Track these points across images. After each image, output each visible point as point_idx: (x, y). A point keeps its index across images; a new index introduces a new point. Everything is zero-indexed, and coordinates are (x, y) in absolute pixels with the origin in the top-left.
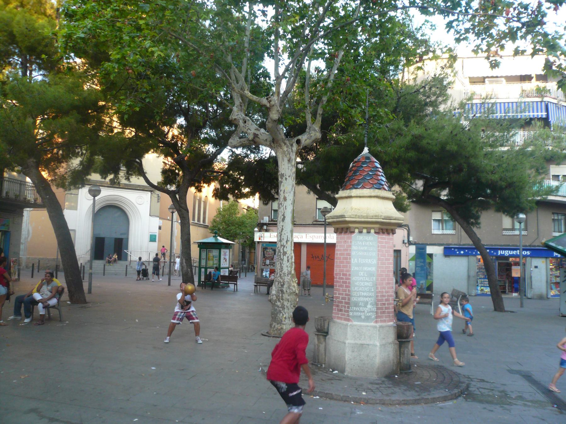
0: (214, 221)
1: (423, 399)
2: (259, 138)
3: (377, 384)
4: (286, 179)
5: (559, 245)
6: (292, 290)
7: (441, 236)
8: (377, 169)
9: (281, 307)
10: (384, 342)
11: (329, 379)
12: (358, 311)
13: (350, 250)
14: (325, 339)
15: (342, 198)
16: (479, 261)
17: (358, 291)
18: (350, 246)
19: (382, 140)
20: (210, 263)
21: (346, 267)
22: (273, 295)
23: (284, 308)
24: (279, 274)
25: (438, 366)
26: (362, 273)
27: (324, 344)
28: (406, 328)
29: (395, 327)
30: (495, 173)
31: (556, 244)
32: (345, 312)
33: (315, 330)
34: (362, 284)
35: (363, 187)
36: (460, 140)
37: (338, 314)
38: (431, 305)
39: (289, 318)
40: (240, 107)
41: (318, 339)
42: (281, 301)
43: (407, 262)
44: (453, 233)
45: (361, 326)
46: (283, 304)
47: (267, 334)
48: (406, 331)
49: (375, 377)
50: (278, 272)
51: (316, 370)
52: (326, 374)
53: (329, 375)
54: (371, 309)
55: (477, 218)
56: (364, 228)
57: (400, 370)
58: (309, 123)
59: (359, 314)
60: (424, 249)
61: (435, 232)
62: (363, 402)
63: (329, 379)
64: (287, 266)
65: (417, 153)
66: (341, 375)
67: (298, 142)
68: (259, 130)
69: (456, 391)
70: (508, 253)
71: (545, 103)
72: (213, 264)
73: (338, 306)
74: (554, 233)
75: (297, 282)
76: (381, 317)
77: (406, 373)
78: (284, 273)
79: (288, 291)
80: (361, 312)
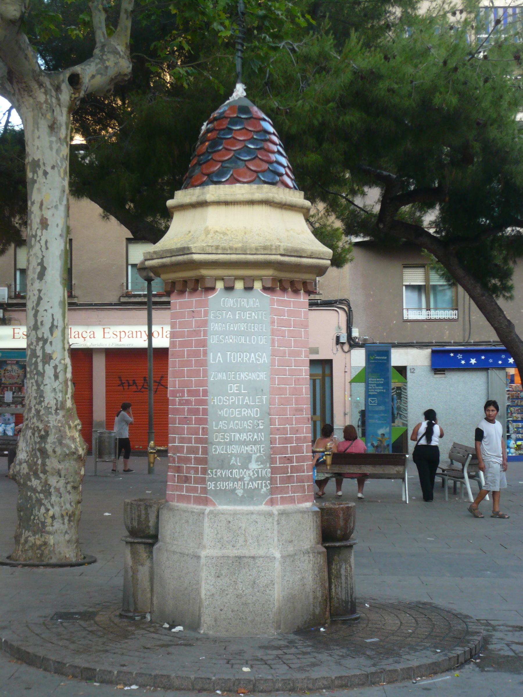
1: (383, 671)
3: (279, 648)
4: (45, 173)
6: (69, 447)
7: (425, 326)
8: (268, 137)
9: (42, 492)
10: (291, 549)
11: (162, 646)
12: (228, 479)
13: (205, 333)
14: (151, 552)
15: (182, 207)
16: (512, 381)
17: (225, 431)
18: (205, 323)
19: (282, 82)
22: (20, 464)
23: (48, 494)
24: (33, 411)
25: (419, 603)
26: (234, 387)
27: (148, 564)
28: (341, 515)
29: (316, 512)
32: (195, 483)
33: (127, 534)
34: (236, 413)
35: (234, 180)
36: (465, 83)
38: (404, 479)
39: (62, 516)
41: (134, 554)
42: (41, 475)
43: (348, 385)
44: (451, 317)
45: (235, 514)
46: (46, 484)
47: (8, 561)
48: (342, 523)
49: (272, 633)
51: (129, 628)
52: (156, 636)
53: (162, 637)
54: (257, 472)
55: (506, 275)
56: (237, 278)
57: (331, 615)
58: (101, 35)
59: (231, 485)
60: (387, 354)
61: (411, 315)
62: (245, 688)
63: (162, 646)
64: (55, 389)
66: (192, 634)
69: (459, 651)
73: (178, 469)
75: (79, 427)
76: (282, 490)
77: (344, 622)
78: (47, 408)
79: (58, 450)
80: (235, 480)
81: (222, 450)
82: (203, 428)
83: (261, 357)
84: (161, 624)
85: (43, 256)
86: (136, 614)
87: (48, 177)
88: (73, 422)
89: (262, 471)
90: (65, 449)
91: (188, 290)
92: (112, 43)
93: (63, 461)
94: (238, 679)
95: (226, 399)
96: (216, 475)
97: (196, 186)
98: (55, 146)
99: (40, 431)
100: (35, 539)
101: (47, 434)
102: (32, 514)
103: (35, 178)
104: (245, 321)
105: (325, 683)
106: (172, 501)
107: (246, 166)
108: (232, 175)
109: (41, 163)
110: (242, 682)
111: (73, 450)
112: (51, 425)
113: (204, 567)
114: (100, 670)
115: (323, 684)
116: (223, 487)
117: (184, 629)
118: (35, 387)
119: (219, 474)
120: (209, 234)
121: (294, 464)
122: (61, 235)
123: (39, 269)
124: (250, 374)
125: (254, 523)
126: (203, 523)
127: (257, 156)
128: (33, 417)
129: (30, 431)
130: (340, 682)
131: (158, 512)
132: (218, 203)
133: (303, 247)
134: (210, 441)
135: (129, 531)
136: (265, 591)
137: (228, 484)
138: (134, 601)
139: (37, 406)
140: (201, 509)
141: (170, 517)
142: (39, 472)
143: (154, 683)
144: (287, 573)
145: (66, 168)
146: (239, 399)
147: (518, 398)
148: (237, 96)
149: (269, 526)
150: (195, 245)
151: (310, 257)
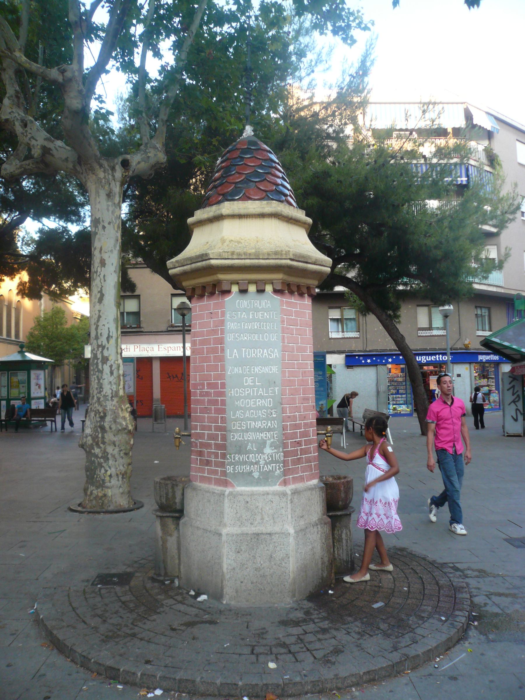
0: (31, 335)
2: (53, 155)
4: (104, 227)
5: (504, 341)
6: (121, 424)
7: (342, 341)
9: (102, 457)
12: (245, 463)
13: (223, 332)
14: (178, 524)
17: (242, 420)
20: (14, 392)
21: (216, 368)
22: (87, 437)
23: (107, 459)
24: (95, 398)
27: (175, 534)
28: (342, 489)
29: (321, 488)
30: (429, 236)
31: (500, 340)
32: (216, 466)
37: (203, 471)
38: (342, 433)
39: (117, 475)
40: (16, 100)
41: (164, 526)
42: (101, 445)
45: (252, 494)
46: (105, 452)
47: (80, 509)
48: (343, 495)
50: (95, 394)
51: (159, 597)
52: (182, 607)
54: (272, 456)
56: (251, 282)
60: (324, 357)
61: (333, 335)
64: (110, 382)
65: (321, 201)
67: (125, 164)
68: (53, 142)
70: (426, 359)
71: (465, 166)
72: (20, 393)
73: (201, 454)
74: (477, 332)
78: (105, 396)
79: (114, 427)
80: (252, 463)
81: (240, 437)
82: (222, 417)
83: (273, 352)
84: (189, 590)
85: (102, 286)
86: (166, 578)
87: (105, 230)
88: (125, 406)
89: (275, 455)
90: (118, 426)
91: (206, 294)
92: (153, 142)
93: (117, 434)
94: (267, 684)
95: (242, 390)
96: (234, 459)
97: (213, 205)
98: (111, 209)
99: (100, 413)
100: (97, 492)
101: (105, 415)
102: (95, 474)
103: (97, 231)
104: (258, 321)
105: (354, 680)
106: (195, 481)
107: (256, 186)
108: (244, 193)
109: (101, 220)
110: (270, 687)
111: (124, 427)
112: (108, 408)
113: (226, 544)
114: (123, 671)
115: (352, 682)
116: (241, 470)
117: (208, 598)
118: (97, 381)
119: (237, 458)
120: (225, 242)
121: (303, 447)
122: (115, 271)
123: (99, 295)
124: (263, 368)
125: (270, 502)
126: (223, 503)
127: (266, 179)
128: (95, 403)
129: (93, 413)
130: (368, 677)
131: (183, 490)
132: (233, 216)
133: (309, 254)
134: (228, 429)
135: (159, 506)
136: (281, 564)
137: (246, 468)
138: (165, 566)
139: (98, 395)
140: (221, 491)
141: (193, 496)
142: (100, 443)
143: (179, 687)
144: (300, 546)
145: (119, 224)
146: (253, 391)
147: (393, 381)
148: (246, 135)
149: (283, 505)
150: (212, 251)
151: (314, 264)
